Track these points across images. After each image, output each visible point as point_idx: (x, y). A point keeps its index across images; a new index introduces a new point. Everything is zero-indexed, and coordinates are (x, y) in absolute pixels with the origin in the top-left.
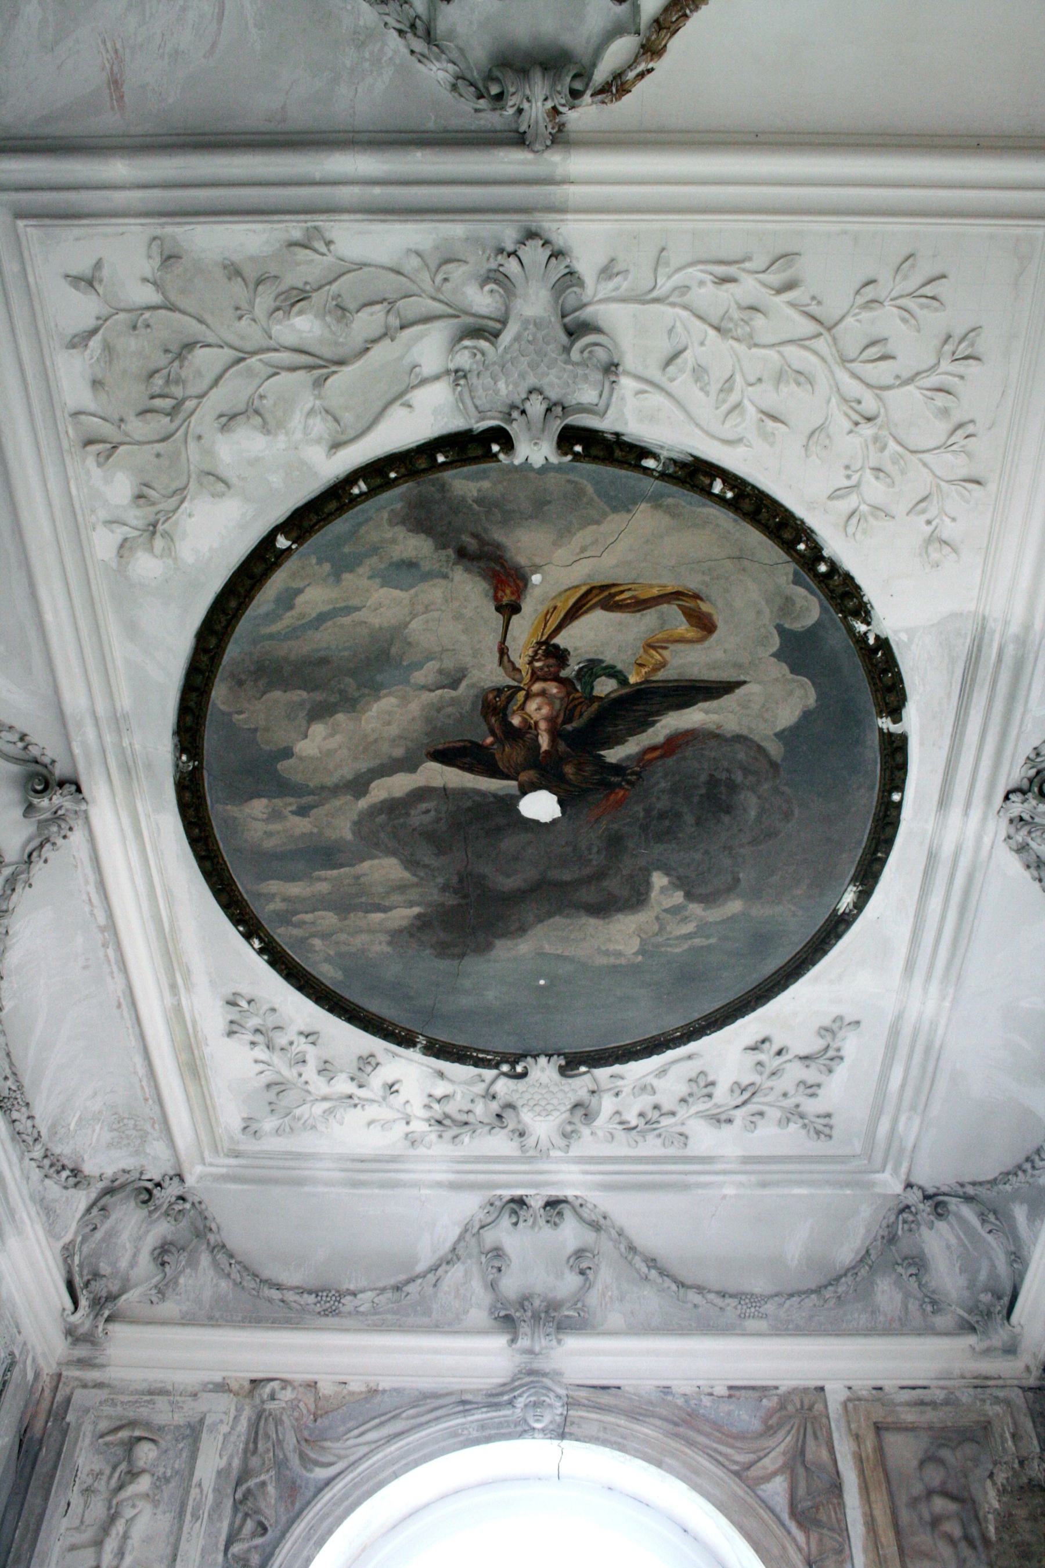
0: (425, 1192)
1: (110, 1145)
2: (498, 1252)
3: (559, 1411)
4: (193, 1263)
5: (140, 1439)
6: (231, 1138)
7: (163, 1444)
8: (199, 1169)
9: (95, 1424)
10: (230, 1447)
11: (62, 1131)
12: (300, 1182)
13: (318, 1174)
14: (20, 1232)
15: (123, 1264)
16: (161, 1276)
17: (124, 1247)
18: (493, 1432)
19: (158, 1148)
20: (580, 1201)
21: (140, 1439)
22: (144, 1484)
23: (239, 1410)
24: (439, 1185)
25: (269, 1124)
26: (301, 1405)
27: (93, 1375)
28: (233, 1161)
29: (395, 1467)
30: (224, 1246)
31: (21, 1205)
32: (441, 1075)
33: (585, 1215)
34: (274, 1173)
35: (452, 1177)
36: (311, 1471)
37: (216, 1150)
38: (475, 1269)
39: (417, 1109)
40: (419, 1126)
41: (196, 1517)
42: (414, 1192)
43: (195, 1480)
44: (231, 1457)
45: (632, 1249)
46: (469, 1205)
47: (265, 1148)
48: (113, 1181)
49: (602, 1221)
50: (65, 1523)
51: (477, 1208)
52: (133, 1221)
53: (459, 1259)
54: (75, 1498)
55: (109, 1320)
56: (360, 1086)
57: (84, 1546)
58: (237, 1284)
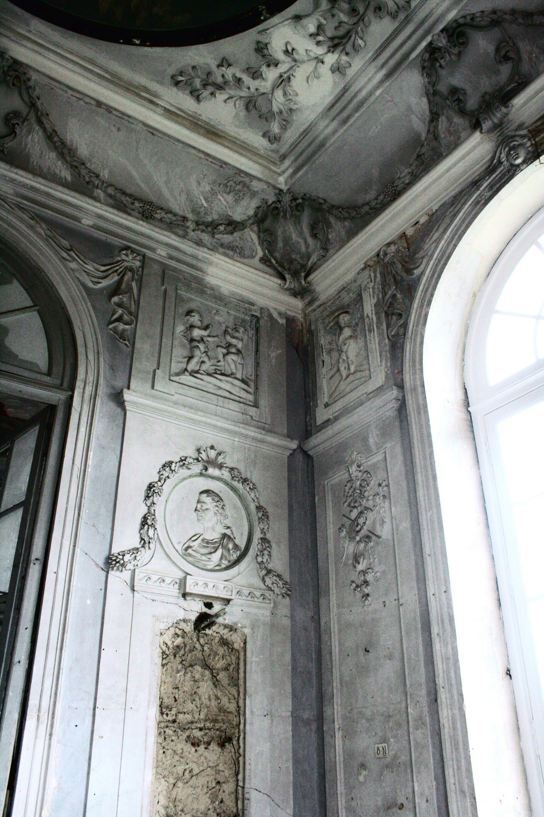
0: (378, 93)
1: (236, 201)
2: (454, 91)
3: (529, 144)
4: (329, 225)
5: (338, 316)
6: (272, 151)
7: (351, 311)
8: (281, 179)
9: (324, 323)
10: (376, 291)
11: (202, 209)
12: (322, 145)
13: (327, 132)
14: (210, 263)
15: (303, 249)
16: (319, 242)
17: (298, 242)
18: (498, 186)
19: (256, 185)
20: (468, 18)
21: (338, 316)
22: (347, 332)
23: (375, 272)
24: (382, 82)
25: (275, 128)
26: (401, 248)
27: (317, 303)
28: (287, 163)
29: (453, 242)
30: (333, 206)
31: (197, 251)
32: (298, 18)
33: (483, 23)
34: (310, 150)
35: (384, 72)
36: (413, 274)
37: (274, 164)
38: (451, 113)
39: (320, 51)
40: (331, 59)
41: (370, 331)
42: (372, 99)
43: (365, 314)
44: (378, 295)
45: (527, 15)
46: (412, 81)
47: (291, 141)
48: (256, 216)
49: (495, 17)
50: (324, 370)
51: (421, 78)
52: (292, 228)
53: (438, 115)
54: (326, 358)
55: (306, 277)
56: (276, 65)
57: (335, 374)
58: (353, 218)
